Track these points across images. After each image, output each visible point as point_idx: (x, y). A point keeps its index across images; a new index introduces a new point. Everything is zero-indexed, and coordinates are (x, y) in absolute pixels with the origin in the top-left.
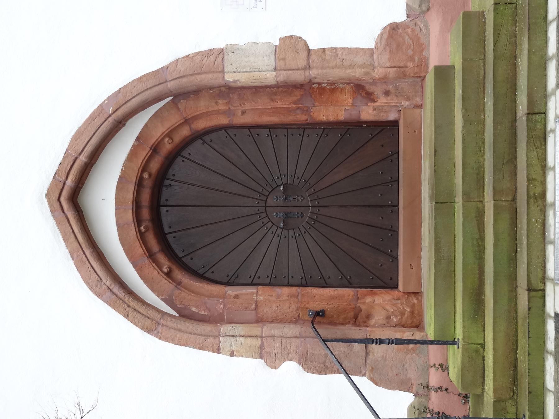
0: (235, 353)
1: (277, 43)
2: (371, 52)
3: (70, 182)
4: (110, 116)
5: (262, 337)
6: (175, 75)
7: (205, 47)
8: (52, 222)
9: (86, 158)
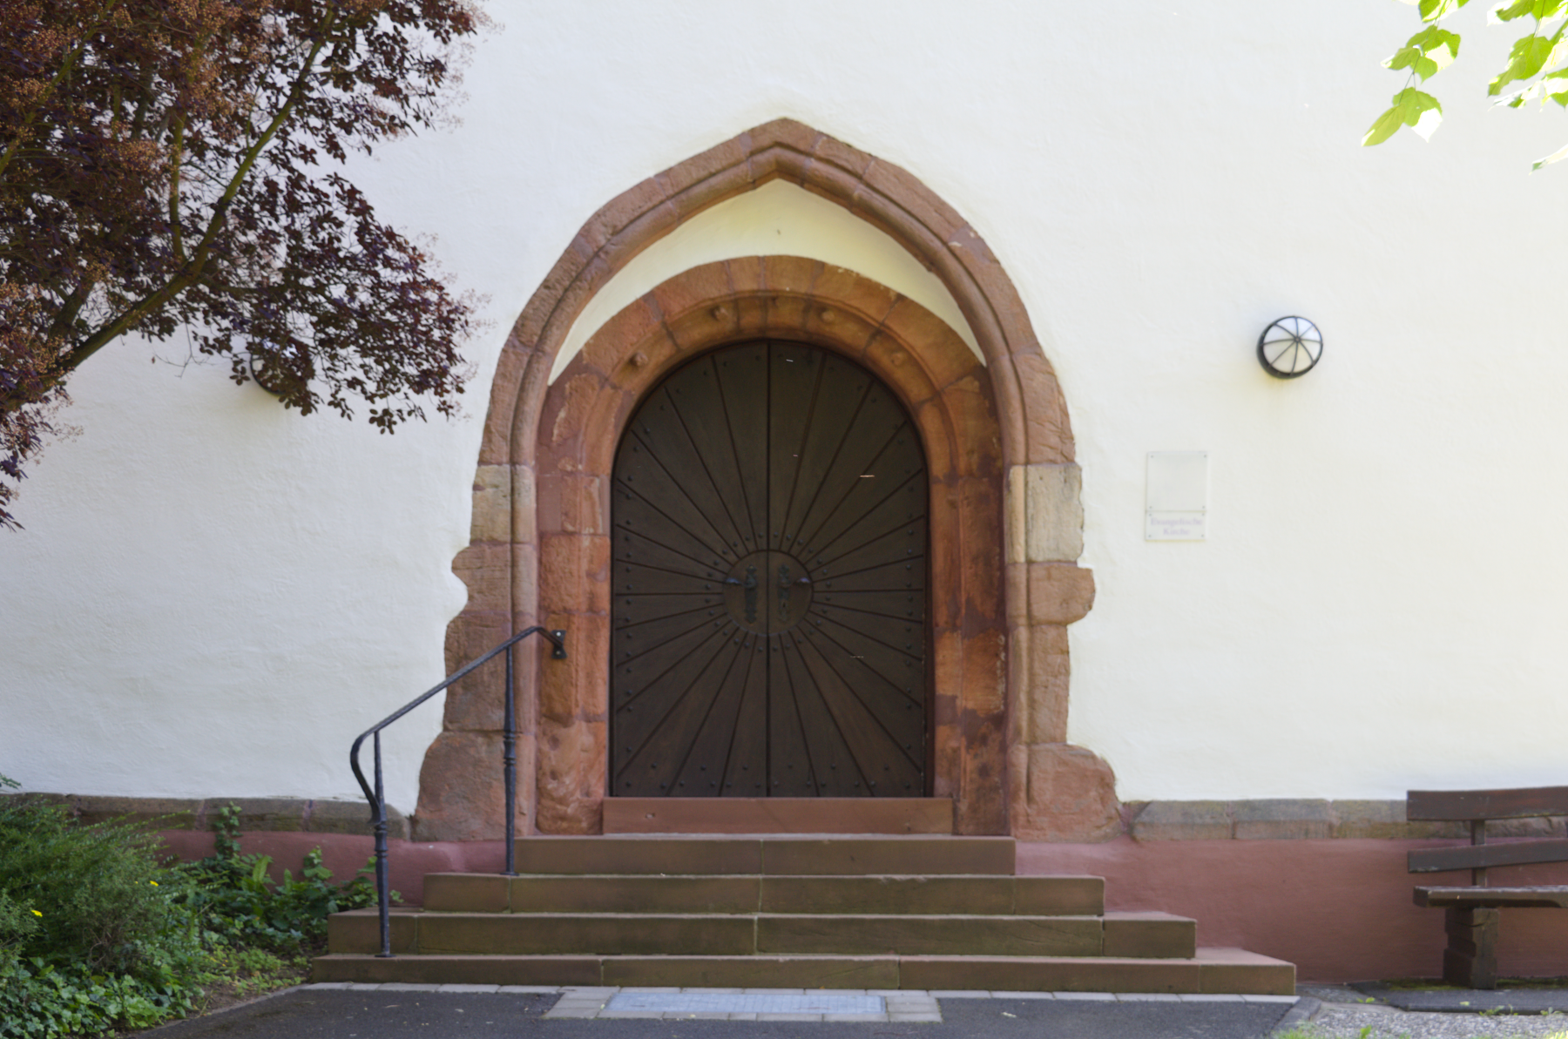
0: (479, 493)
1: (1081, 564)
2: (1061, 739)
3: (812, 164)
4: (945, 243)
5: (768, 550)
6: (1022, 368)
7: (1077, 425)
8: (730, 131)
9: (860, 198)
